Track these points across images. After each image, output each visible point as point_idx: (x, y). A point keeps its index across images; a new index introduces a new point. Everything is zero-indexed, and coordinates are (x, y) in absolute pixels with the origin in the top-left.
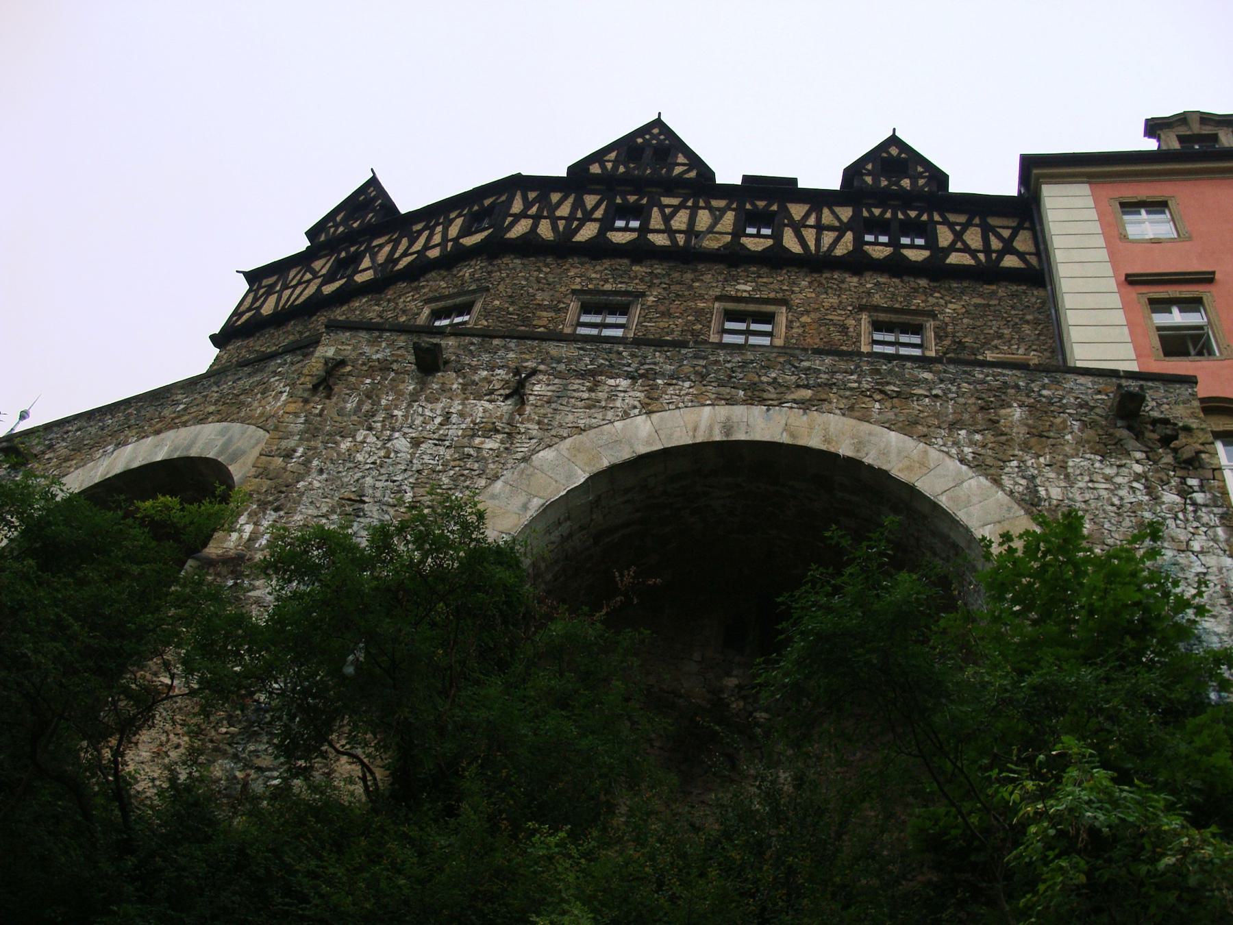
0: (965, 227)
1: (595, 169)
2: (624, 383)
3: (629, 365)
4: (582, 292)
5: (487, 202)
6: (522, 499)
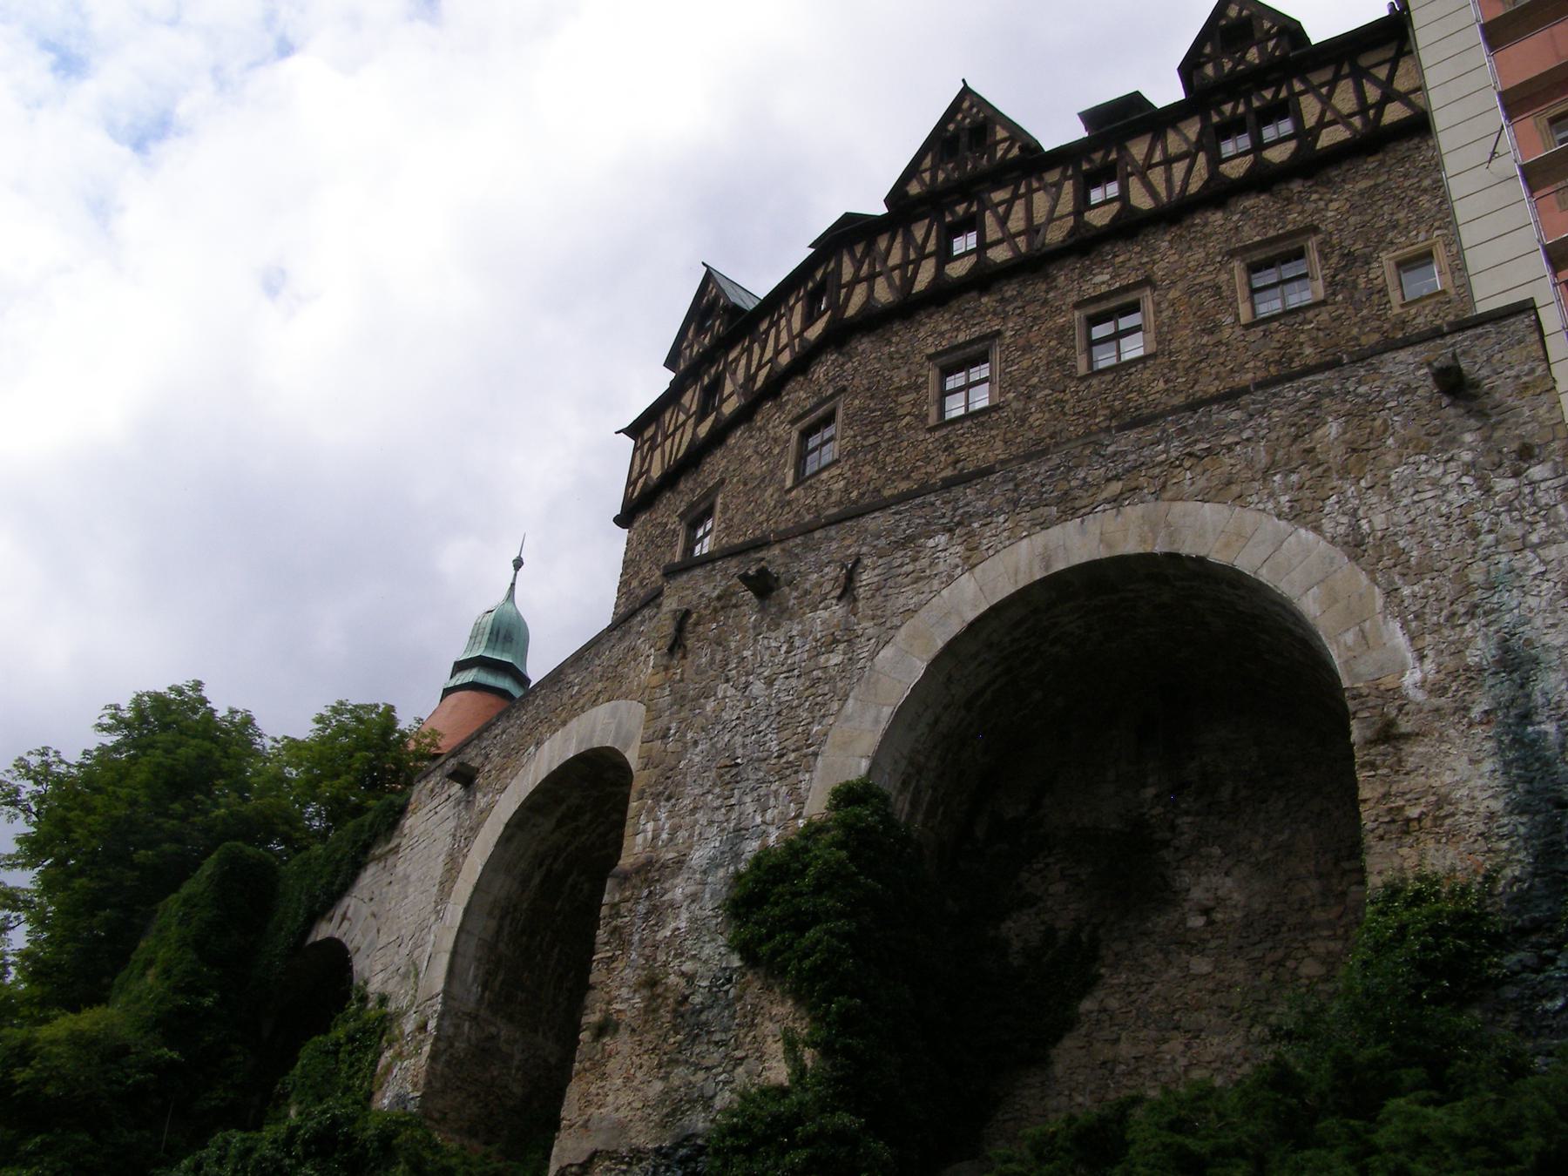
1: (914, 189)
2: (942, 539)
3: (944, 516)
4: (938, 354)
5: (819, 275)
6: (872, 712)
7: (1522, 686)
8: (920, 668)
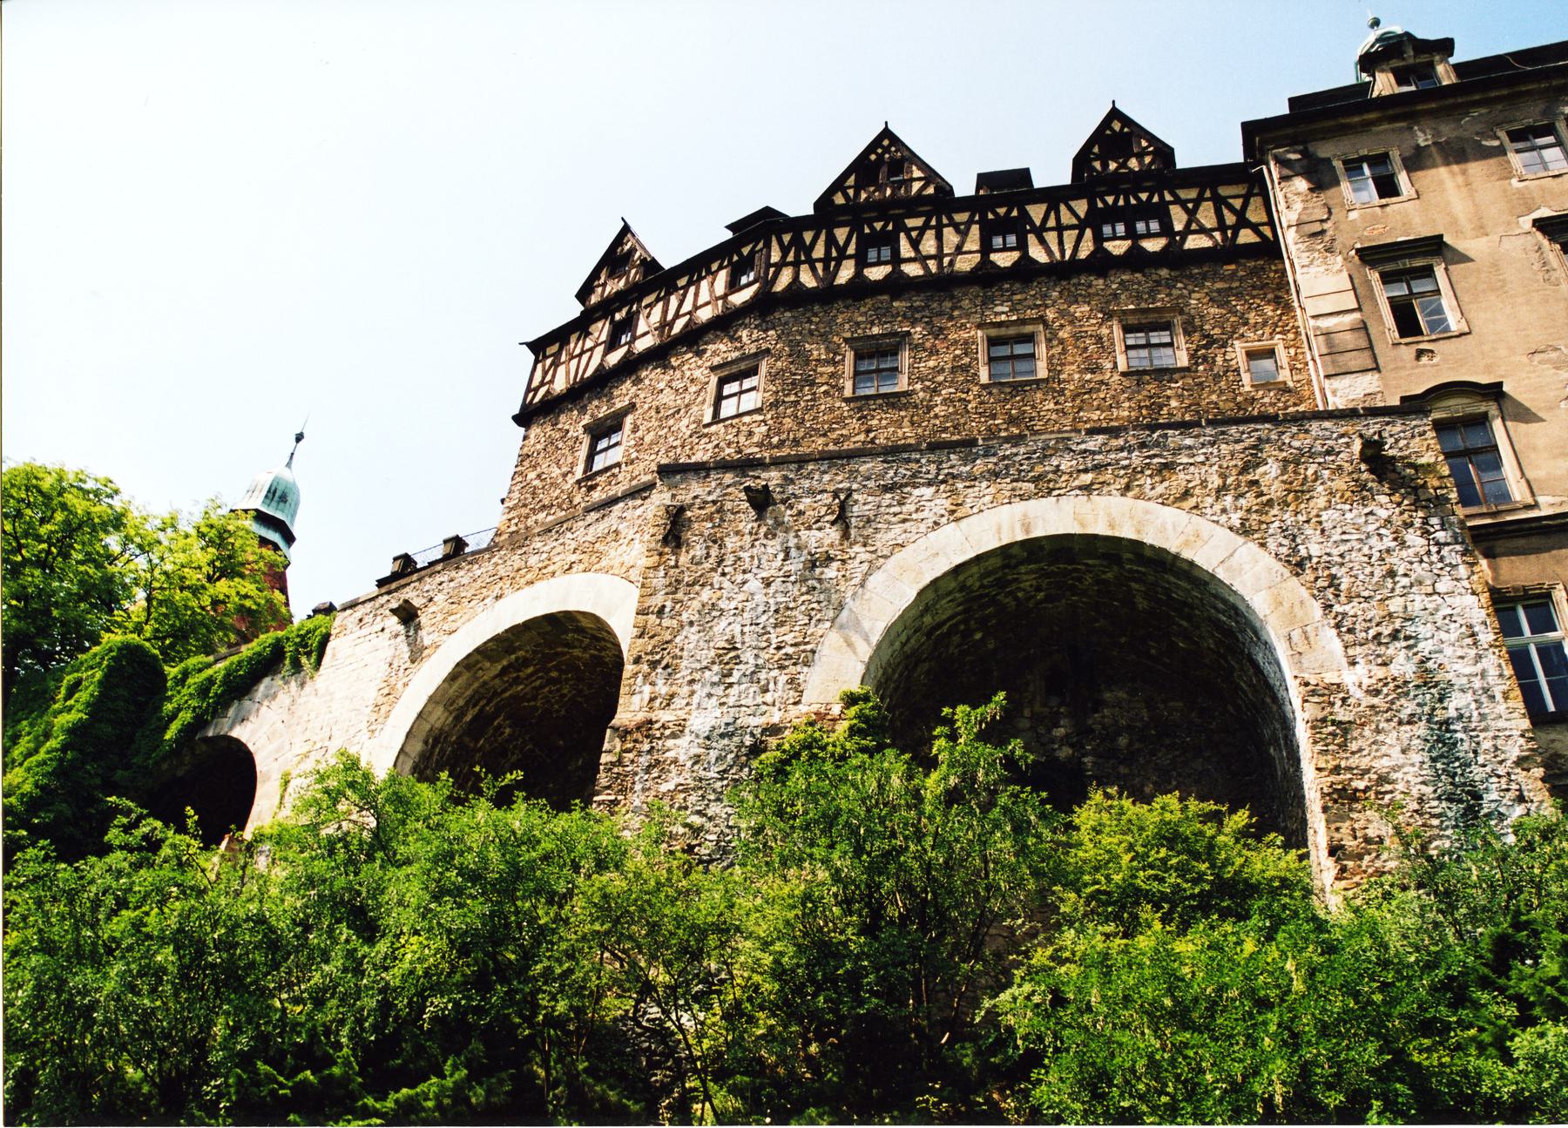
0: (1198, 202)
2: (928, 492)
4: (852, 339)
5: (746, 251)
7: (1441, 701)
8: (911, 595)
